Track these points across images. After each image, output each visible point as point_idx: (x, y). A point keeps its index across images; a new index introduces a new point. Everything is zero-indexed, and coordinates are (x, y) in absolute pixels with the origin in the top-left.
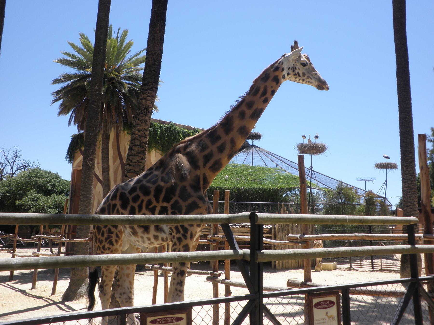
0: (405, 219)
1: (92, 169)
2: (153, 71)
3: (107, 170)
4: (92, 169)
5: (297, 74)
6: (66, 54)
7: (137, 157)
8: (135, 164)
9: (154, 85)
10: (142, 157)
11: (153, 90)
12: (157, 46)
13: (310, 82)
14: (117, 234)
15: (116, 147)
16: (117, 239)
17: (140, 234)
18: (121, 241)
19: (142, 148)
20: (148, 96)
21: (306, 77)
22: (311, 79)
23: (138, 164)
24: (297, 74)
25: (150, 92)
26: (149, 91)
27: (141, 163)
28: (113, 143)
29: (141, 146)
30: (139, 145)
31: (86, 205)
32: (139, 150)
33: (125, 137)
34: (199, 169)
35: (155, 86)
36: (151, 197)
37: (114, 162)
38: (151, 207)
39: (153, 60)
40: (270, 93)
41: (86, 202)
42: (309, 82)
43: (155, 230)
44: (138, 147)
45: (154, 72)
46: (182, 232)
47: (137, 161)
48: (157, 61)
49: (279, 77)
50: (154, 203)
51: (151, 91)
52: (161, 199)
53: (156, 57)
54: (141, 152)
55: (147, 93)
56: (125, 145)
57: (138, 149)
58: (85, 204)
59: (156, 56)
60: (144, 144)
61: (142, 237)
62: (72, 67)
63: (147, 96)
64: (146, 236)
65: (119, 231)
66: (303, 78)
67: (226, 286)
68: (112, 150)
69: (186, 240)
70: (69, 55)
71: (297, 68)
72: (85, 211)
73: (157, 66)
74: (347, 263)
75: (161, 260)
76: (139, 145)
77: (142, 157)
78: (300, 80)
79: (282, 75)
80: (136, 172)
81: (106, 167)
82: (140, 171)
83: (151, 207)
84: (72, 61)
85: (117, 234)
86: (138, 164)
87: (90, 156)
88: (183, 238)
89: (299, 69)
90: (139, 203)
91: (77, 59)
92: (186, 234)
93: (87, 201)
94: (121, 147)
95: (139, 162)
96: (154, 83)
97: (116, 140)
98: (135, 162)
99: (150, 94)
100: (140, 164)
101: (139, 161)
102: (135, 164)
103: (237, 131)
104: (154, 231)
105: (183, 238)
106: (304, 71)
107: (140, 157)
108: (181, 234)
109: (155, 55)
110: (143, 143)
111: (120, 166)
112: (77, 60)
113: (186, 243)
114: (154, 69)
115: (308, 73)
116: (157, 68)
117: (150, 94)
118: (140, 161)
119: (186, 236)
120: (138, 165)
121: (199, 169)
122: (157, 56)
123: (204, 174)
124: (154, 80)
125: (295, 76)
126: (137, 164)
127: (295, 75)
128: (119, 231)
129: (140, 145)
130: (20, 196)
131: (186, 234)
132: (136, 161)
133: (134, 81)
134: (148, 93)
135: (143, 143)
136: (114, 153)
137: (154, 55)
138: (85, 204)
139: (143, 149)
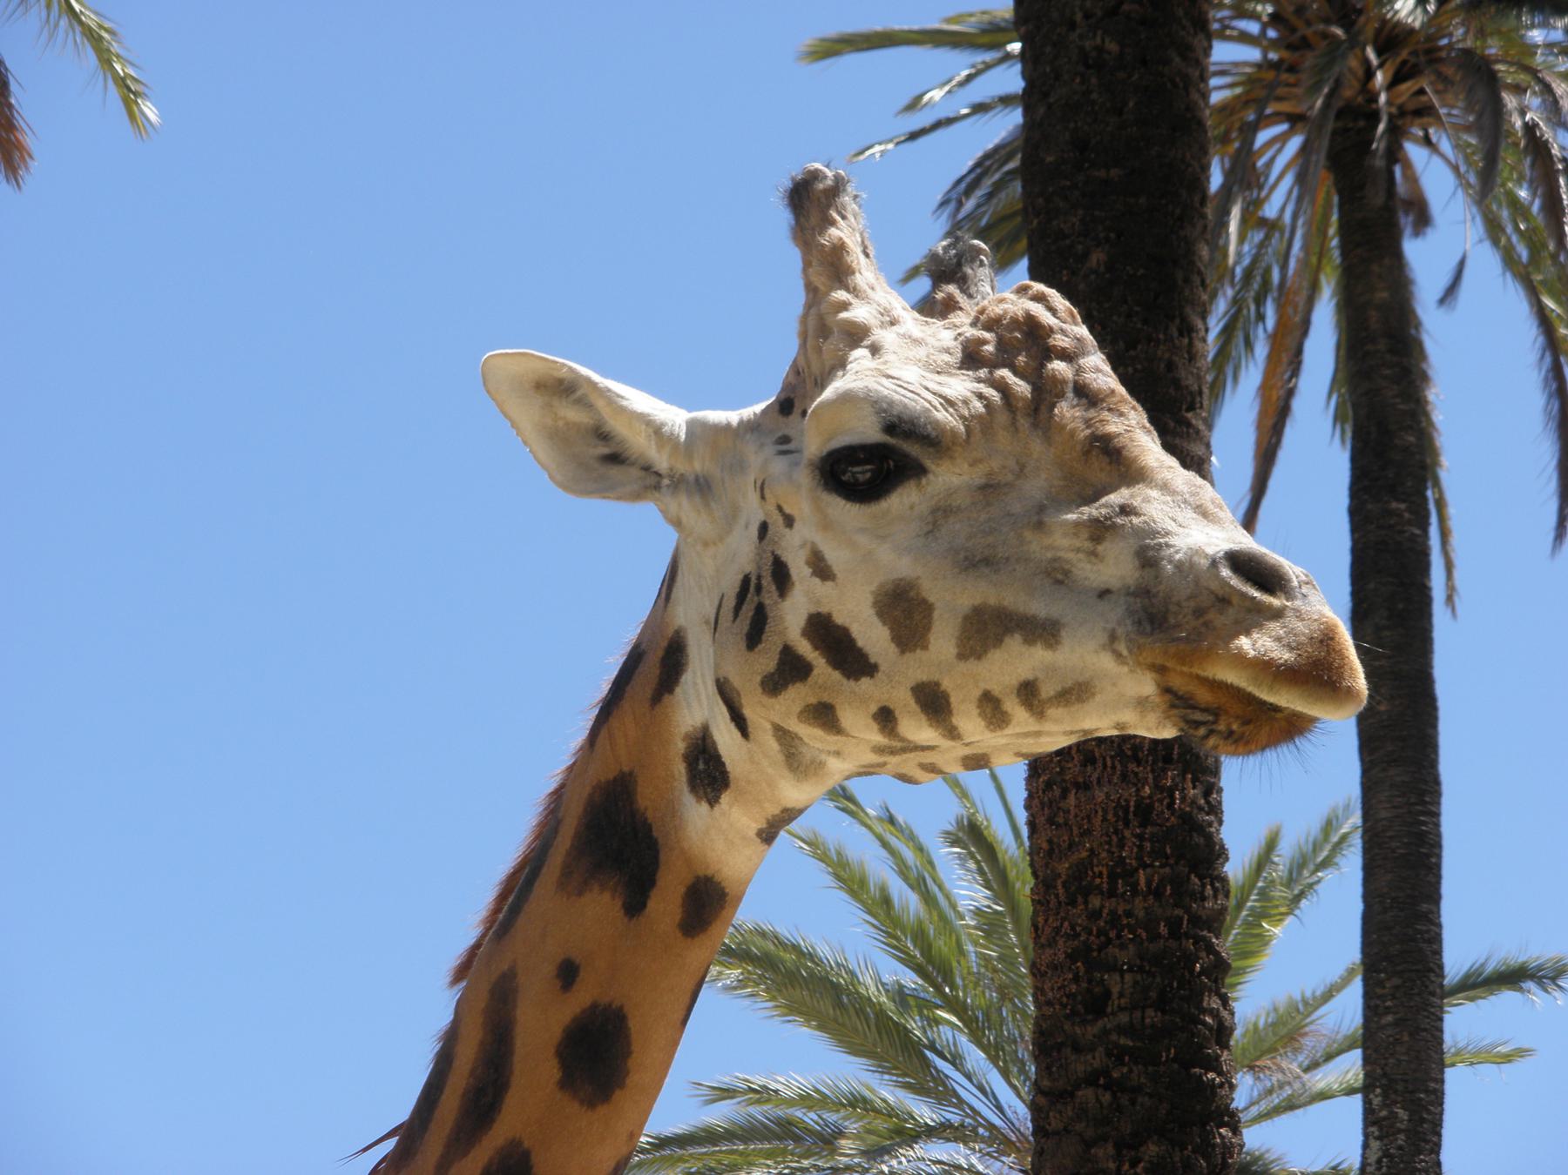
2: (1091, 1080)
5: (805, 648)
12: (1085, 787)
13: (1047, 690)
21: (943, 641)
22: (1044, 632)
24: (805, 648)
39: (1072, 957)
40: (550, 1070)
42: (1028, 692)
45: (1107, 1098)
48: (1112, 950)
49: (646, 798)
53: (1095, 915)
59: (1096, 902)
66: (917, 668)
71: (799, 568)
73: (1124, 1018)
78: (886, 718)
79: (681, 746)
89: (822, 570)
106: (897, 563)
109: (1087, 892)
114: (1097, 1059)
115: (976, 563)
122: (1112, 893)
125: (796, 696)
127: (791, 669)
137: (1072, 902)
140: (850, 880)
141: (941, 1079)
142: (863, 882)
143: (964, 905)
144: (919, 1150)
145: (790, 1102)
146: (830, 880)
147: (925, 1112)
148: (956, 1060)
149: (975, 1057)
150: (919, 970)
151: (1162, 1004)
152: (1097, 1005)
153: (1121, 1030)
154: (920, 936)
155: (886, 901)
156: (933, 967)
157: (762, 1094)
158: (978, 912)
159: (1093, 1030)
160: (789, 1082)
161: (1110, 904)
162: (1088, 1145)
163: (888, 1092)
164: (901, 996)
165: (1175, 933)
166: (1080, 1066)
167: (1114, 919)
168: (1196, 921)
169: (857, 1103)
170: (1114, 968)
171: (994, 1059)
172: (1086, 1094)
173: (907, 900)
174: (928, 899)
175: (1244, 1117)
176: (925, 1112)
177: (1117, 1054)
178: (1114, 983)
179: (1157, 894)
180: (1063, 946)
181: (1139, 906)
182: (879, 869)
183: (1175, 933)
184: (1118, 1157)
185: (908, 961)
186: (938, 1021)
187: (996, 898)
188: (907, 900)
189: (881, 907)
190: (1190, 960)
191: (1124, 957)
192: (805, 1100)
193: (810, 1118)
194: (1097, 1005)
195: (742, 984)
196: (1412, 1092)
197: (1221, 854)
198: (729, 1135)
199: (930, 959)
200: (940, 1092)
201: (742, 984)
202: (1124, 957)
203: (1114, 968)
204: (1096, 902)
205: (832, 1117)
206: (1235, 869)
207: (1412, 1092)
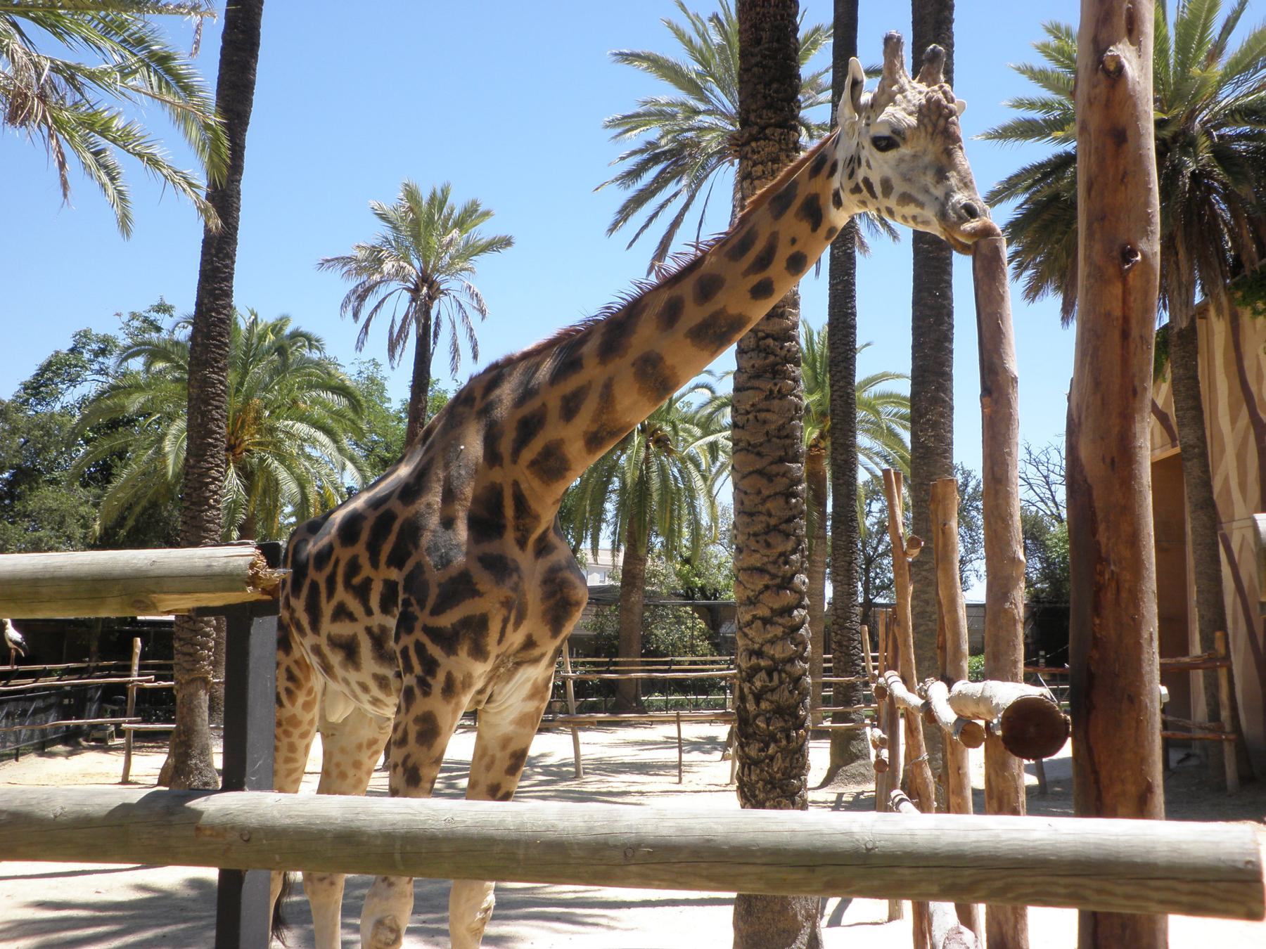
0: (85, 570)
1: (938, 454)
2: (756, 65)
3: (1196, 450)
4: (938, 454)
6: (1019, 104)
7: (750, 393)
8: (746, 418)
9: (764, 116)
10: (771, 391)
11: (765, 135)
14: (288, 670)
15: (1234, 368)
16: (290, 685)
17: (339, 671)
18: (304, 691)
19: (765, 358)
20: (755, 165)
23: (756, 417)
25: (758, 147)
26: (753, 144)
27: (768, 411)
28: (1225, 354)
29: (760, 351)
30: (753, 350)
31: (926, 578)
32: (753, 366)
33: (1255, 328)
34: (501, 465)
35: (771, 118)
36: (360, 549)
37: (1234, 421)
38: (356, 580)
39: (751, 27)
41: (926, 567)
43: (373, 658)
44: (749, 355)
46: (418, 669)
47: (753, 405)
48: (764, 24)
50: (367, 571)
51: (762, 143)
52: (383, 557)
53: (758, 13)
54: (765, 372)
55: (749, 155)
56: (1258, 356)
57: (750, 364)
58: (924, 573)
59: (758, 9)
60: (770, 341)
61: (347, 682)
62: (1039, 140)
63: (750, 163)
64: (353, 676)
65: (296, 662)
67: (746, 911)
68: (1225, 380)
69: (426, 699)
70: (1032, 105)
72: (926, 597)
73: (767, 46)
74: (645, 881)
75: (1095, 772)
76: (753, 350)
77: (771, 391)
80: (754, 446)
81: (1191, 442)
82: (769, 441)
83: (356, 580)
84: (1045, 120)
85: (288, 670)
86: (756, 417)
87: (926, 414)
88: (417, 692)
90: (328, 570)
91: (1057, 109)
92: (429, 679)
93: (926, 563)
94: (1247, 364)
95: (759, 411)
96: (765, 111)
97: (1231, 344)
98: (748, 413)
99: (759, 152)
100: (762, 416)
101: (761, 406)
102: (748, 420)
103: (633, 364)
104: (373, 661)
105: (417, 692)
107: (761, 389)
108: (416, 676)
109: (755, 6)
110: (767, 336)
111: (1252, 431)
112: (1059, 112)
113: (427, 709)
114: (758, 59)
116: (767, 53)
117: (759, 152)
118: (763, 405)
119: (429, 686)
120: (758, 421)
121: (501, 465)
122: (763, 6)
123: (516, 484)
124: (765, 97)
126: (751, 416)
128: (296, 662)
129: (758, 346)
130: (270, 553)
131: (429, 679)
132: (748, 407)
133: (1243, 119)
134: (754, 152)
135: (767, 336)
136: (1230, 389)
137: (751, 9)
138: (924, 573)
139: (767, 361)
140: (679, 34)
141: (707, 97)
142: (684, 35)
143: (715, 42)
144: (701, 117)
145: (663, 105)
146: (674, 35)
147: (702, 107)
148: (712, 92)
149: (717, 91)
150: (701, 64)
151: (778, 41)
152: (758, 42)
153: (765, 49)
154: (701, 52)
155: (691, 41)
156: (704, 62)
157: (656, 103)
158: (718, 44)
159: (757, 50)
160: (663, 99)
161: (762, 10)
162: (755, 85)
163: (692, 102)
164: (698, 74)
165: (782, 16)
166: (754, 61)
167: (764, 15)
168: (788, 15)
169: (683, 104)
170: (763, 30)
171: (722, 91)
172: (755, 69)
173: (698, 41)
174: (705, 41)
175: (803, 105)
176: (702, 107)
177: (764, 57)
178: (763, 34)
179: (777, 6)
180: (748, 24)
181: (771, 11)
182: (690, 31)
183: (782, 16)
184: (765, 88)
185: (697, 60)
186: (707, 81)
187: (723, 40)
188: (698, 41)
189: (689, 43)
190: (786, 27)
191: (767, 26)
192: (668, 104)
193: (668, 110)
194: (758, 42)
195: (648, 68)
196: (714, 614)
197: (796, 29)
198: (644, 115)
199: (703, 57)
200: (708, 101)
201: (648, 68)
202: (767, 26)
203: (763, 30)
204: (758, 9)
205: (676, 109)
206: (801, 35)
207: (714, 614)
